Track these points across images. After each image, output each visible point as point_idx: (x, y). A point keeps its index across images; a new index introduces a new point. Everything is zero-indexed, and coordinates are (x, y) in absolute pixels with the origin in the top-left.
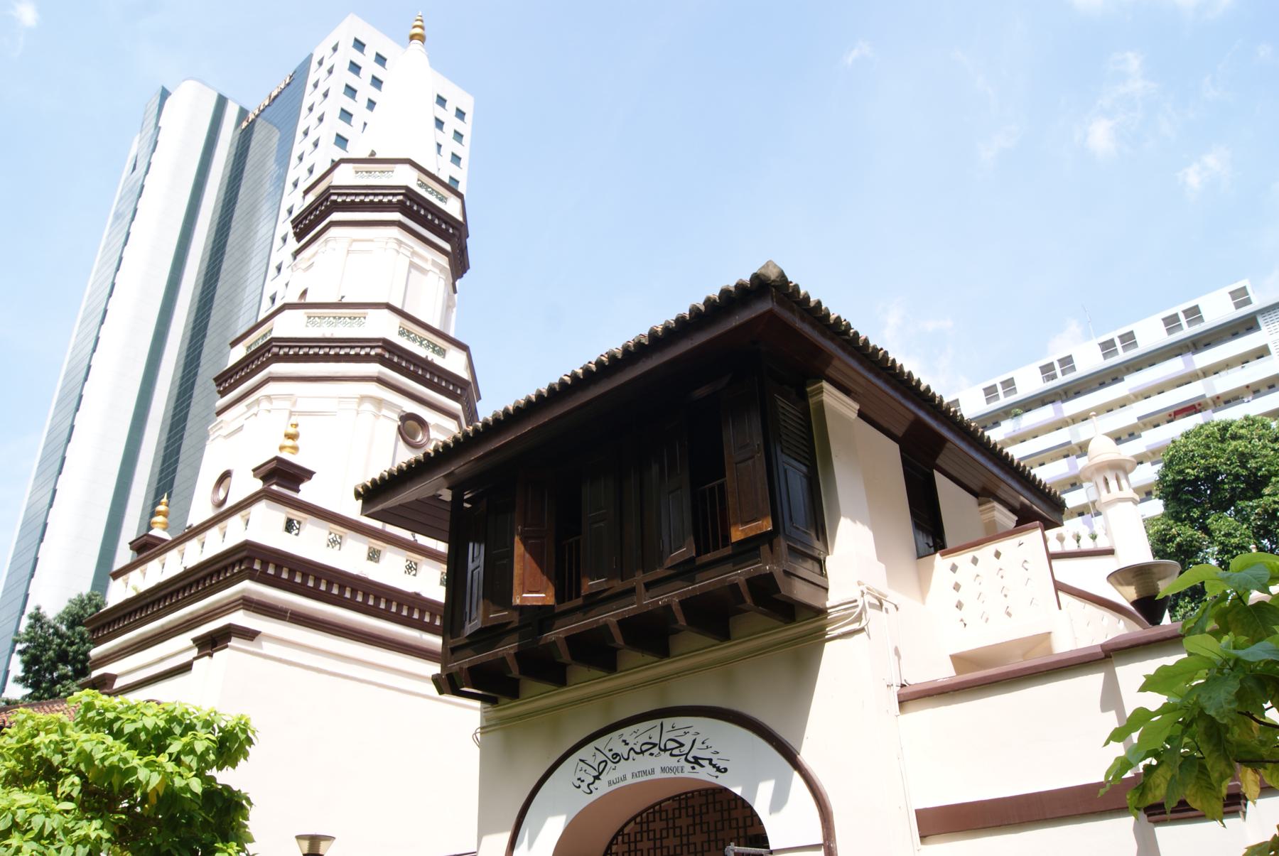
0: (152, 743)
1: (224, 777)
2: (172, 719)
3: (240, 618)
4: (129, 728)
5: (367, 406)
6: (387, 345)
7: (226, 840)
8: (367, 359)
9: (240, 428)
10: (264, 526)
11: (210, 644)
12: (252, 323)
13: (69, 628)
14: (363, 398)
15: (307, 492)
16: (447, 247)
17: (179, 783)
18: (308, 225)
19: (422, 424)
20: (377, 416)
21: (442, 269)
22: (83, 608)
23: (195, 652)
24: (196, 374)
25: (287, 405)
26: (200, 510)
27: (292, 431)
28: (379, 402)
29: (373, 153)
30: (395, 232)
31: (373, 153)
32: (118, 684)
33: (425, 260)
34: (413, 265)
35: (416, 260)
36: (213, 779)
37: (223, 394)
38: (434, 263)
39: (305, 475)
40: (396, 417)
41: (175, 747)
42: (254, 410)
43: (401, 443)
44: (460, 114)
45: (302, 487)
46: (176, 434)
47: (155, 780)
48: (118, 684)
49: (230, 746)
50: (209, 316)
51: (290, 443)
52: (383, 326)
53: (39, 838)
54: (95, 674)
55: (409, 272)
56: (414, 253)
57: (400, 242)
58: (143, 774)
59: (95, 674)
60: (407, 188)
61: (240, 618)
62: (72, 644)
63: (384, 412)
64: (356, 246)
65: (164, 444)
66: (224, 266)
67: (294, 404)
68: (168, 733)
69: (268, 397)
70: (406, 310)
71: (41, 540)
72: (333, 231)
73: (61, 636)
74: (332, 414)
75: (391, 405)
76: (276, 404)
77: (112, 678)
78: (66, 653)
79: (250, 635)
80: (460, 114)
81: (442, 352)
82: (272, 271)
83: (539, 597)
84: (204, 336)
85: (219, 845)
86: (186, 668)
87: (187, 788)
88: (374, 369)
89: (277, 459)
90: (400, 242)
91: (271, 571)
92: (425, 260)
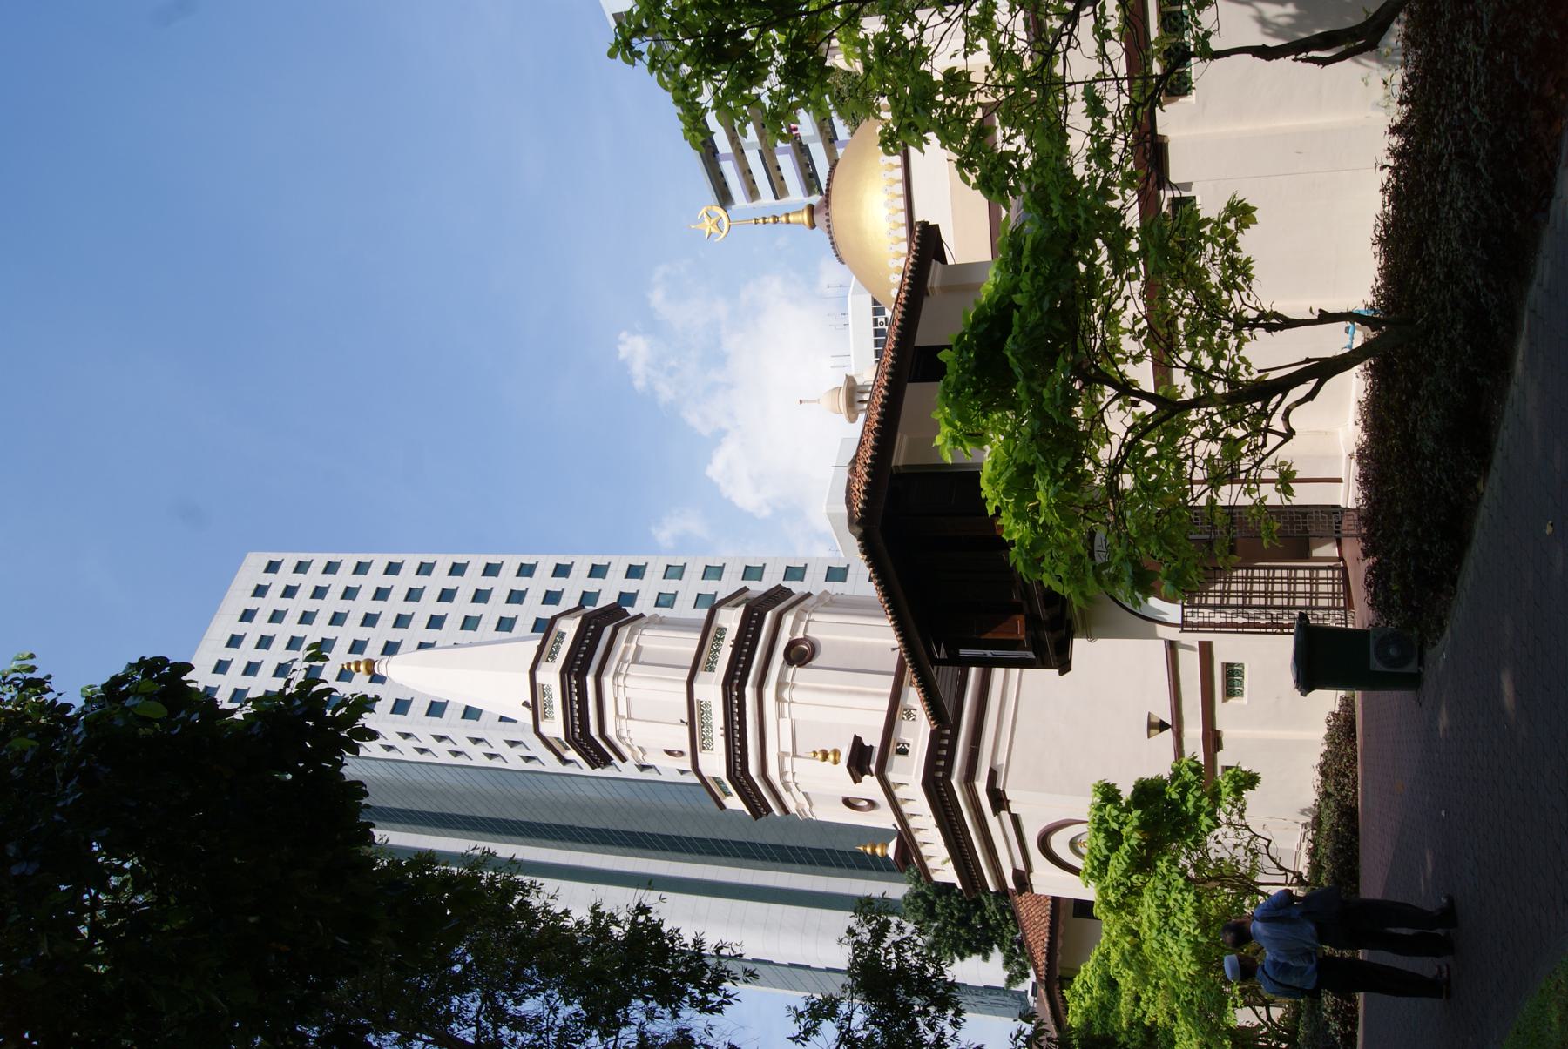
0: (1114, 839)
1: (1126, 793)
2: (1098, 830)
3: (981, 786)
4: (1105, 852)
5: (786, 694)
6: (727, 683)
7: (1164, 792)
8: (742, 697)
9: (805, 794)
10: (909, 773)
11: (999, 801)
12: (704, 790)
13: (936, 920)
14: (779, 698)
15: (873, 740)
16: (608, 630)
17: (1136, 823)
18: (597, 753)
19: (792, 645)
20: (793, 686)
21: (632, 633)
22: (917, 910)
23: (1004, 814)
24: (616, 832)
25: (788, 761)
26: (884, 819)
27: (820, 756)
28: (781, 685)
29: (525, 704)
30: (607, 681)
31: (525, 704)
32: (1021, 866)
33: (626, 650)
34: (635, 661)
35: (630, 656)
36: (1128, 803)
37: (769, 810)
38: (629, 640)
39: (857, 741)
40: (791, 670)
41: (1115, 826)
42: (792, 785)
43: (813, 663)
44: (273, 567)
45: (867, 744)
46: (720, 848)
47: (1136, 835)
48: (1021, 866)
49: (1109, 794)
50: (548, 825)
51: (831, 757)
52: (710, 690)
53: (1169, 892)
54: (1011, 885)
55: (642, 663)
56: (622, 660)
57: (617, 674)
58: (1133, 842)
59: (1011, 885)
60: (562, 672)
61: (981, 786)
62: (952, 915)
63: (789, 679)
64: (623, 711)
65: (696, 856)
66: (455, 811)
67: (786, 754)
68: (1106, 831)
69: (782, 775)
70: (690, 663)
71: (808, 967)
72: (611, 732)
73: (945, 925)
74: (793, 722)
75: (782, 675)
76: (788, 768)
77: (1016, 873)
78: (960, 919)
79: (993, 774)
80: (273, 567)
81: (722, 631)
82: (425, 758)
83: (1020, 621)
84: (572, 827)
85: (1299, 892)
86: (1015, 819)
87: (1139, 818)
88: (750, 692)
89: (849, 767)
90: (617, 674)
91: (942, 763)
92: (626, 650)
